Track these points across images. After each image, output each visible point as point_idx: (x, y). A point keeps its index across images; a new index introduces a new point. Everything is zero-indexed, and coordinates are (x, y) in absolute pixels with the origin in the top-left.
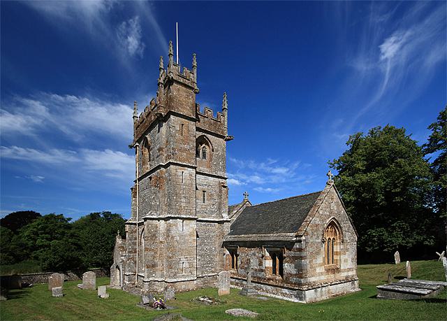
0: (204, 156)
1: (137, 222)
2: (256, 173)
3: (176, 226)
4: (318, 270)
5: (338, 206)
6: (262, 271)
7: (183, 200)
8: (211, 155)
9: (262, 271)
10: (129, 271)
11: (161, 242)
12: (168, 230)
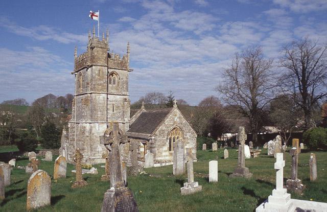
0: (114, 83)
1: (76, 122)
2: (270, 33)
3: (95, 127)
4: (164, 154)
5: (180, 118)
6: (139, 153)
7: (99, 113)
8: (118, 82)
9: (139, 153)
10: (71, 152)
11: (87, 136)
12: (91, 130)
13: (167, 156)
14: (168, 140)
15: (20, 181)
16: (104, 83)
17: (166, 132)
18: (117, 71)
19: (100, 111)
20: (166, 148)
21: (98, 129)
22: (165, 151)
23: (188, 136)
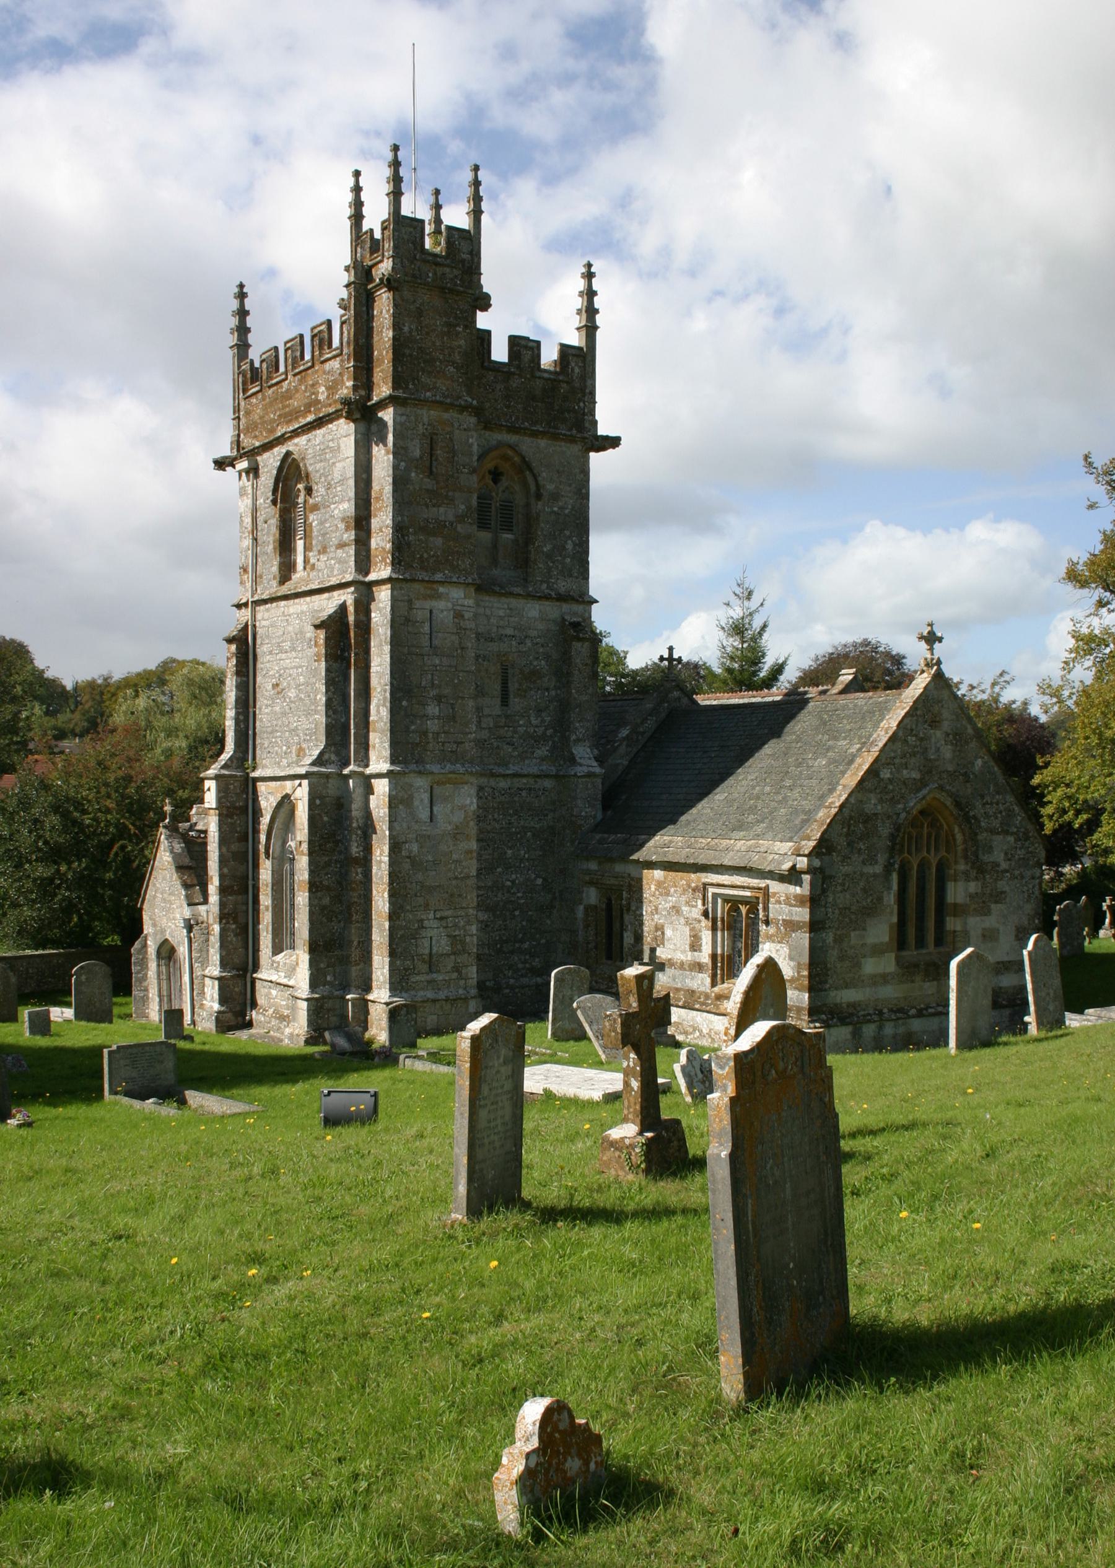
4: (870, 966)
7: (433, 709)
13: (884, 979)
14: (895, 877)
15: (910, 1126)
16: (461, 519)
17: (885, 830)
18: (529, 446)
19: (439, 699)
20: (880, 931)
21: (424, 815)
22: (878, 951)
23: (998, 856)
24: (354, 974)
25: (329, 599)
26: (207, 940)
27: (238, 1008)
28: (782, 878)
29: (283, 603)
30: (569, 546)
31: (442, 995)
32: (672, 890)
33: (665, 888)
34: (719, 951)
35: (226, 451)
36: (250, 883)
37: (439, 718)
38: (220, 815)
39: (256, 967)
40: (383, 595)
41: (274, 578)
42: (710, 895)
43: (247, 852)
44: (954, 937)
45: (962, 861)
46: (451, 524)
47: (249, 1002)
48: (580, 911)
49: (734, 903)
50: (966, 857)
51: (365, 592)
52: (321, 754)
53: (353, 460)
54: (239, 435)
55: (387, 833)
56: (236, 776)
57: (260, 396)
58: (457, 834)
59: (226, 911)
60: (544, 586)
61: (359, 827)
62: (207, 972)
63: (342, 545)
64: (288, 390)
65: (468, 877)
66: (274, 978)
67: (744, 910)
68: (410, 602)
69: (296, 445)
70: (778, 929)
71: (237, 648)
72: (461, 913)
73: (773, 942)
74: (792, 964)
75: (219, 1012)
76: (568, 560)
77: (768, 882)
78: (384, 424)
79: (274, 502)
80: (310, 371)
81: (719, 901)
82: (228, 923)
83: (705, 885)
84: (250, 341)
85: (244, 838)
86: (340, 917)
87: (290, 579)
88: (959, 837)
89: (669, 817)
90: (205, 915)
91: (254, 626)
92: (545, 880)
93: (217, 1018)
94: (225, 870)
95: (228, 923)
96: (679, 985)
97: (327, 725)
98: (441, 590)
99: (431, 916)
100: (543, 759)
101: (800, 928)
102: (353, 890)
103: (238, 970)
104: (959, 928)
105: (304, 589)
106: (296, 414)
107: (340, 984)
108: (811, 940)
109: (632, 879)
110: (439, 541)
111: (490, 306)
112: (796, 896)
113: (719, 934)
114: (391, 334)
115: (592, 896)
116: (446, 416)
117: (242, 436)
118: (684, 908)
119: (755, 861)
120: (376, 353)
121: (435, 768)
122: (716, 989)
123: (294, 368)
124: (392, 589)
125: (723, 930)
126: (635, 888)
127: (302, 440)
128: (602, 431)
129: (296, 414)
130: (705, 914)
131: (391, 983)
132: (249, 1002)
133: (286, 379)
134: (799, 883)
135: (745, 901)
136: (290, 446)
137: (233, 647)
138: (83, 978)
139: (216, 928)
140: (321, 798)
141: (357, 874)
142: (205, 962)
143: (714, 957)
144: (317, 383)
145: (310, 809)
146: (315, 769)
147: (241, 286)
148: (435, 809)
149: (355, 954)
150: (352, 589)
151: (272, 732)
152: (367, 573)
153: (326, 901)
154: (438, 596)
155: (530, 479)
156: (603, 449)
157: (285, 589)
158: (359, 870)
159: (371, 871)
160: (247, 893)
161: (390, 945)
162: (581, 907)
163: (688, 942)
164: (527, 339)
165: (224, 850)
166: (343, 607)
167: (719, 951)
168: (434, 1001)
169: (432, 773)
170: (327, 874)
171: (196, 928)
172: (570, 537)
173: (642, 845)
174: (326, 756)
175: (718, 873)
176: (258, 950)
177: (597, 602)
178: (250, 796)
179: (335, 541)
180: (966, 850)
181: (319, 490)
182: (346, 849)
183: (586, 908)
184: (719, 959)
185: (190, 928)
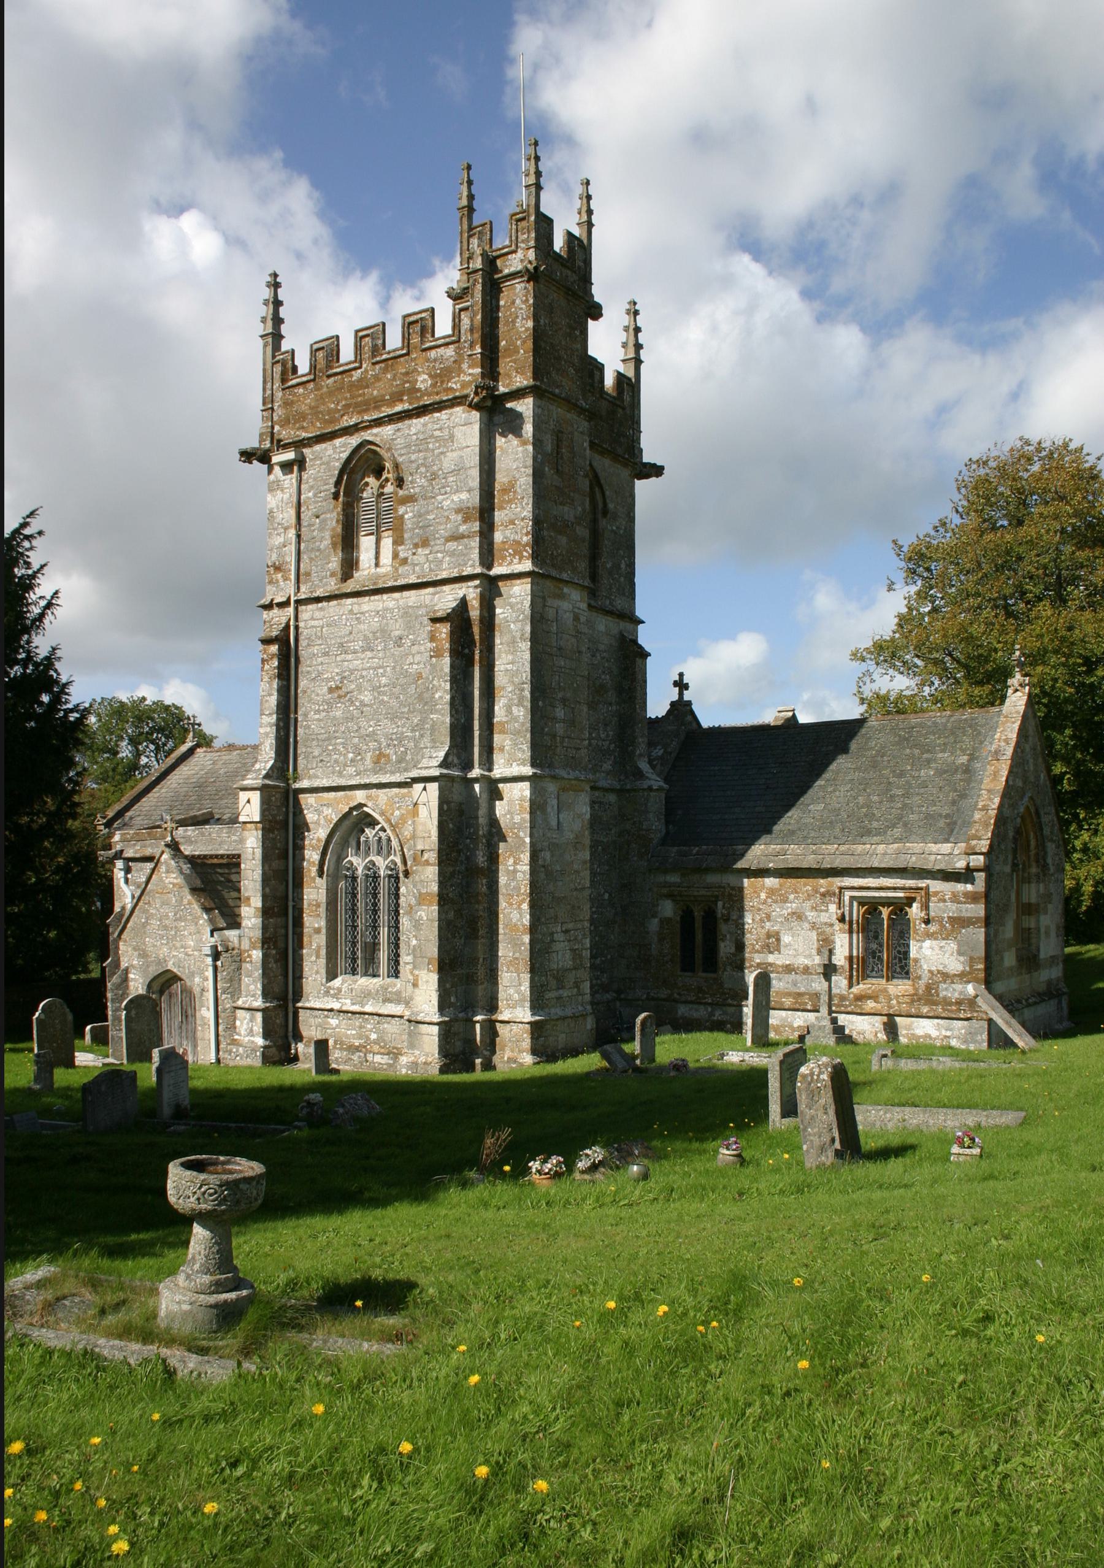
7: (560, 713)
24: (480, 994)
25: (434, 594)
26: (239, 968)
27: (280, 1042)
28: (948, 876)
29: (349, 601)
30: (623, 566)
31: (569, 1012)
32: (792, 897)
33: (781, 895)
34: (855, 953)
35: (252, 442)
36: (291, 904)
37: (564, 721)
38: (263, 829)
39: (298, 995)
40: (519, 594)
41: (333, 575)
42: (847, 899)
43: (287, 870)
44: (1029, 934)
45: (1034, 864)
46: (573, 524)
47: (290, 1034)
48: (654, 925)
49: (872, 907)
50: (1037, 861)
51: (491, 587)
52: (447, 755)
53: (477, 449)
54: (273, 427)
55: (528, 840)
56: (278, 787)
57: (311, 385)
58: (577, 844)
59: (267, 935)
60: (608, 602)
61: (484, 836)
62: (240, 1003)
63: (456, 537)
64: (360, 380)
65: (583, 889)
66: (336, 1006)
67: (885, 912)
68: (544, 598)
69: (376, 435)
70: (942, 926)
71: (279, 649)
72: (579, 926)
73: (936, 939)
74: (962, 959)
75: (265, 1047)
76: (622, 579)
77: (928, 881)
78: (519, 416)
79: (336, 496)
80: (402, 359)
81: (855, 904)
82: (269, 948)
83: (841, 888)
84: (283, 333)
85: (284, 855)
86: (462, 932)
87: (352, 577)
88: (1033, 843)
89: (763, 827)
90: (236, 940)
91: (297, 628)
92: (610, 895)
93: (263, 1054)
94: (267, 890)
95: (269, 948)
96: (803, 990)
97: (451, 725)
98: (566, 590)
99: (559, 929)
100: (608, 773)
101: (973, 924)
102: (478, 902)
103: (278, 999)
104: (1033, 925)
105: (390, 584)
106: (378, 403)
107: (461, 1006)
108: (987, 935)
109: (733, 888)
110: (563, 540)
111: (601, 315)
112: (966, 894)
113: (855, 936)
114: (530, 324)
115: (668, 909)
116: (569, 416)
117: (277, 428)
118: (808, 914)
119: (913, 862)
120: (503, 343)
121: (563, 773)
122: (855, 990)
123: (374, 356)
124: (532, 584)
125: (858, 933)
126: (736, 899)
127: (388, 430)
128: (646, 459)
129: (378, 403)
130: (842, 919)
131: (531, 1001)
132: (290, 1034)
133: (360, 367)
134: (972, 881)
135: (887, 903)
136: (367, 435)
137: (274, 649)
138: (133, 1012)
139: (257, 955)
140: (448, 803)
141: (482, 886)
142: (235, 991)
143: (850, 959)
144: (415, 370)
145: (440, 815)
146: (445, 771)
147: (275, 275)
148: (561, 816)
149: (481, 972)
150: (477, 582)
151: (328, 739)
152: (490, 567)
153: (451, 915)
154: (562, 596)
155: (598, 496)
156: (647, 476)
157: (350, 586)
158: (484, 881)
159: (497, 882)
160: (286, 915)
161: (531, 961)
162: (656, 920)
163: (815, 946)
164: (596, 360)
165: (267, 868)
166: (464, 602)
167: (855, 953)
168: (564, 1018)
169: (563, 778)
170: (452, 886)
171: (224, 955)
172: (623, 557)
173: (742, 855)
174: (450, 759)
175: (858, 877)
176: (301, 977)
177: (643, 622)
178: (291, 809)
179: (443, 531)
180: (1037, 854)
181: (416, 483)
182: (468, 858)
183: (661, 921)
184: (855, 960)
185: (216, 955)
